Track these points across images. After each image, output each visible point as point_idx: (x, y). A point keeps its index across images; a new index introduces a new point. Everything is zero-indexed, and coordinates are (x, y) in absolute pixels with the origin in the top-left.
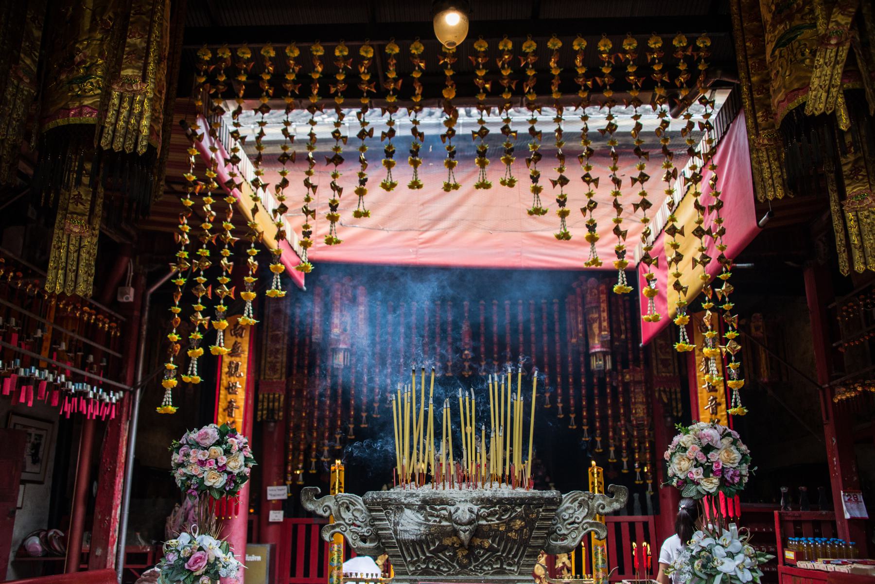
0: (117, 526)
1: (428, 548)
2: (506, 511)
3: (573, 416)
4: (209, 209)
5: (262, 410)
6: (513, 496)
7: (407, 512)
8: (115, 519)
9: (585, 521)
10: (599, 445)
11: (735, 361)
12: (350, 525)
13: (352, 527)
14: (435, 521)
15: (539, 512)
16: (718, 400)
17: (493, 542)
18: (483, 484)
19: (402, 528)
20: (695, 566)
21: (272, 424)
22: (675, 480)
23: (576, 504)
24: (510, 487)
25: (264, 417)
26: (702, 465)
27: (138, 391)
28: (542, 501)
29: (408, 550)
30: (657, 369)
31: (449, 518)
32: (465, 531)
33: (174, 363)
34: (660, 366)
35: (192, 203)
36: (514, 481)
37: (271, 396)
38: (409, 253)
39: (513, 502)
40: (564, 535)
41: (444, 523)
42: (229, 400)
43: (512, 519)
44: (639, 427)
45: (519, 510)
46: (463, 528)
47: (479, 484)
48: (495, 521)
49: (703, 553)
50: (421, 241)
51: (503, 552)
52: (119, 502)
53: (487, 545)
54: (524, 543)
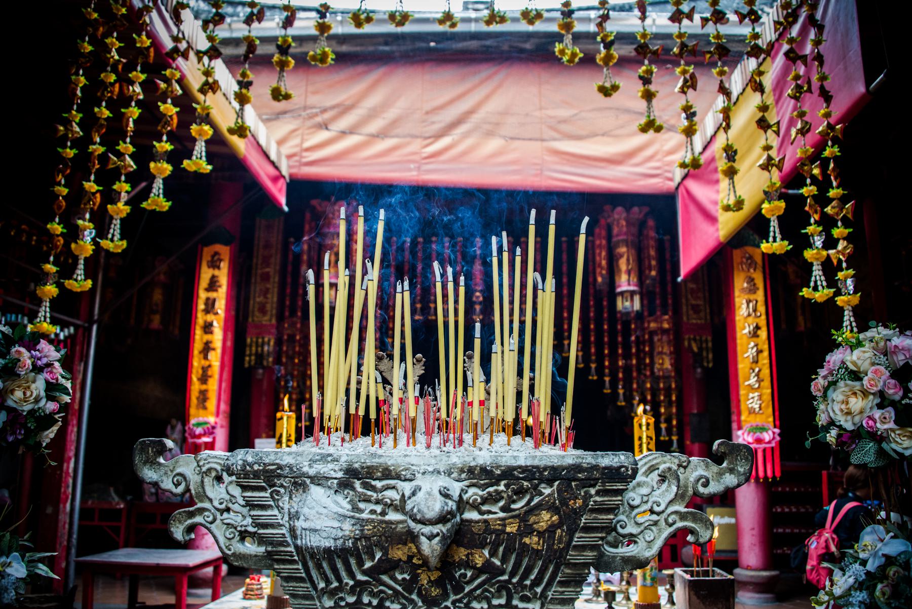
0: (71, 481)
1: (360, 563)
2: (520, 492)
3: (593, 366)
4: (117, 57)
5: (250, 355)
6: (536, 462)
7: (316, 491)
8: (67, 473)
9: (672, 509)
10: (621, 397)
11: (847, 269)
12: (222, 512)
13: (225, 515)
14: (373, 512)
15: (588, 496)
16: (759, 347)
17: (493, 554)
18: (476, 438)
19: (305, 525)
20: (878, 593)
21: (261, 371)
22: (834, 432)
23: (655, 476)
24: (530, 442)
25: (253, 363)
26: (893, 404)
27: (95, 328)
28: (596, 474)
29: (319, 567)
30: (688, 315)
31: (400, 507)
32: (431, 537)
33: (54, 264)
34: (691, 312)
35: (90, 48)
36: (537, 433)
37: (260, 340)
38: (410, 170)
39: (535, 475)
40: (632, 535)
41: (393, 516)
42: (205, 341)
43: (532, 510)
44: (666, 378)
45: (547, 491)
46: (427, 530)
47: (468, 438)
48: (496, 512)
49: (891, 571)
50: (424, 155)
51: (512, 574)
52: (72, 454)
53: (479, 562)
54: (556, 558)
